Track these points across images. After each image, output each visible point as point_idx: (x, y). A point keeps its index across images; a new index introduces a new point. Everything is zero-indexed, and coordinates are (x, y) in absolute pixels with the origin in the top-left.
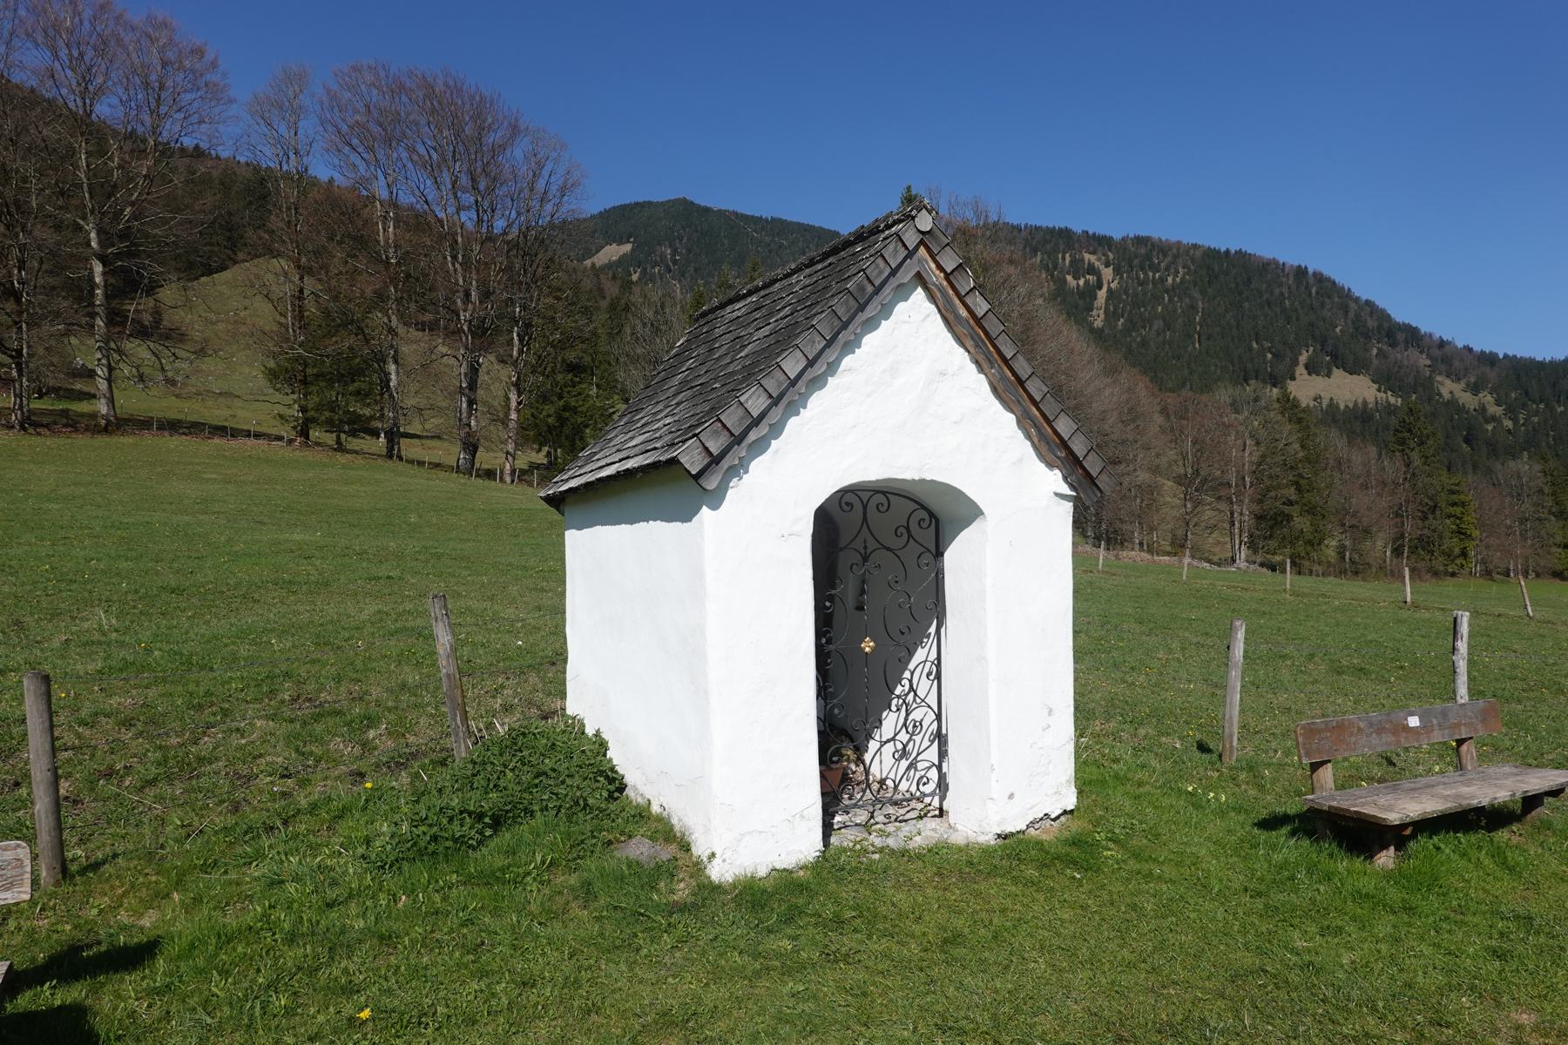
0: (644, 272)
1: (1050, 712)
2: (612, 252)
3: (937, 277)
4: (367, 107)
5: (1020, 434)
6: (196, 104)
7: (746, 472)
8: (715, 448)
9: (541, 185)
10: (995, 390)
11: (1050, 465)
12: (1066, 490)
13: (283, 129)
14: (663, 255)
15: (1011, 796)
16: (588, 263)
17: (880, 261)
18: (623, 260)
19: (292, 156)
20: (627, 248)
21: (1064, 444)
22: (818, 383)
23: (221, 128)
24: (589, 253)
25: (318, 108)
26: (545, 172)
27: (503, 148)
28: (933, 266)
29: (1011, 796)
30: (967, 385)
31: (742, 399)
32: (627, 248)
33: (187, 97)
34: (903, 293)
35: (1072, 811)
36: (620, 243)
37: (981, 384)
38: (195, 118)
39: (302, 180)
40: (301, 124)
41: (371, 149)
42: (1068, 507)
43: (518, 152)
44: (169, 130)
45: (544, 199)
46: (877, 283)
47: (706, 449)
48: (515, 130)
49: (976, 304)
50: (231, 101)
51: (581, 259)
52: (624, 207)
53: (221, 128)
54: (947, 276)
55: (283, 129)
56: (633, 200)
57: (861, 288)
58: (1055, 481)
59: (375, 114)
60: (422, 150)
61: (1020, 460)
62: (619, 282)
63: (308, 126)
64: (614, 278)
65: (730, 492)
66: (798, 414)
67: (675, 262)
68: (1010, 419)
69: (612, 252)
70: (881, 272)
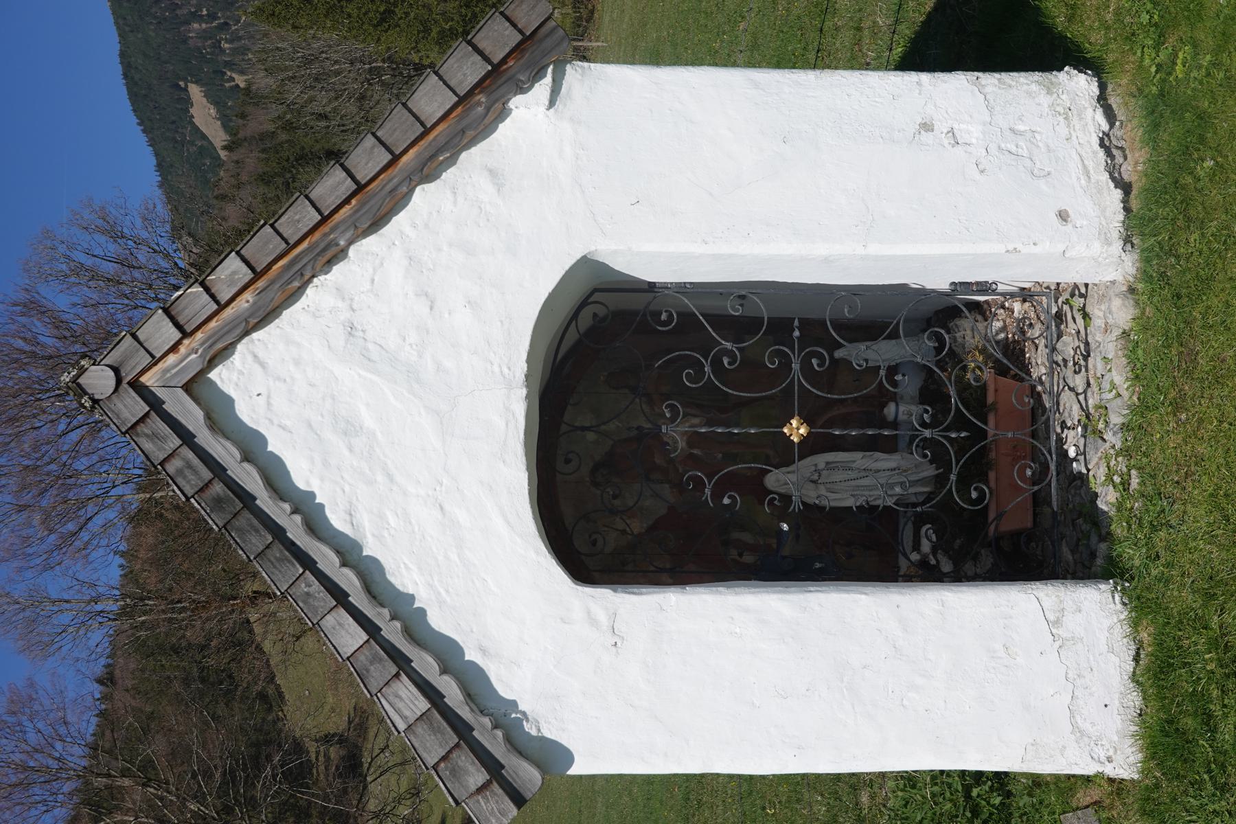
0: (230, 65)
1: (927, 127)
2: (204, 114)
3: (189, 357)
4: (21, 508)
5: (449, 175)
6: (40, 725)
7: (514, 704)
8: (477, 776)
9: (110, 268)
10: (377, 223)
11: (503, 114)
12: (543, 87)
13: (65, 618)
14: (204, 36)
15: (1063, 216)
16: (223, 154)
17: (171, 468)
18: (215, 99)
19: (99, 607)
20: (195, 91)
21: (463, 100)
22: (371, 575)
23: (71, 695)
24: (207, 149)
25: (29, 574)
26: (89, 262)
27: (58, 323)
28: (172, 359)
29: (1063, 216)
30: (374, 279)
31: (402, 726)
32: (195, 91)
33: (32, 737)
34: (220, 414)
35: (1102, 87)
36: (188, 102)
37: (365, 250)
38: (62, 730)
39: (134, 598)
40: (54, 596)
41: (82, 504)
42: (575, 73)
43: (60, 300)
44: (77, 756)
45: (126, 263)
46: (206, 474)
47: (480, 790)
48: (33, 306)
49: (231, 281)
50: (31, 684)
51: (218, 163)
52: (134, 97)
53: (71, 695)
54: (185, 334)
55: (65, 618)
56: (120, 81)
57: (218, 503)
58: (528, 110)
59: (27, 498)
60: (74, 436)
61: (493, 173)
62: (250, 109)
63: (55, 584)
64: (243, 116)
65: (547, 734)
66: (422, 612)
67: (212, 16)
68: (423, 196)
69: (204, 114)
70: (189, 465)
